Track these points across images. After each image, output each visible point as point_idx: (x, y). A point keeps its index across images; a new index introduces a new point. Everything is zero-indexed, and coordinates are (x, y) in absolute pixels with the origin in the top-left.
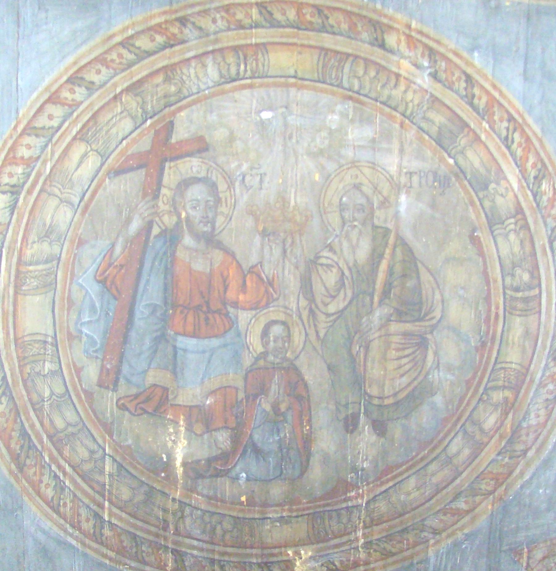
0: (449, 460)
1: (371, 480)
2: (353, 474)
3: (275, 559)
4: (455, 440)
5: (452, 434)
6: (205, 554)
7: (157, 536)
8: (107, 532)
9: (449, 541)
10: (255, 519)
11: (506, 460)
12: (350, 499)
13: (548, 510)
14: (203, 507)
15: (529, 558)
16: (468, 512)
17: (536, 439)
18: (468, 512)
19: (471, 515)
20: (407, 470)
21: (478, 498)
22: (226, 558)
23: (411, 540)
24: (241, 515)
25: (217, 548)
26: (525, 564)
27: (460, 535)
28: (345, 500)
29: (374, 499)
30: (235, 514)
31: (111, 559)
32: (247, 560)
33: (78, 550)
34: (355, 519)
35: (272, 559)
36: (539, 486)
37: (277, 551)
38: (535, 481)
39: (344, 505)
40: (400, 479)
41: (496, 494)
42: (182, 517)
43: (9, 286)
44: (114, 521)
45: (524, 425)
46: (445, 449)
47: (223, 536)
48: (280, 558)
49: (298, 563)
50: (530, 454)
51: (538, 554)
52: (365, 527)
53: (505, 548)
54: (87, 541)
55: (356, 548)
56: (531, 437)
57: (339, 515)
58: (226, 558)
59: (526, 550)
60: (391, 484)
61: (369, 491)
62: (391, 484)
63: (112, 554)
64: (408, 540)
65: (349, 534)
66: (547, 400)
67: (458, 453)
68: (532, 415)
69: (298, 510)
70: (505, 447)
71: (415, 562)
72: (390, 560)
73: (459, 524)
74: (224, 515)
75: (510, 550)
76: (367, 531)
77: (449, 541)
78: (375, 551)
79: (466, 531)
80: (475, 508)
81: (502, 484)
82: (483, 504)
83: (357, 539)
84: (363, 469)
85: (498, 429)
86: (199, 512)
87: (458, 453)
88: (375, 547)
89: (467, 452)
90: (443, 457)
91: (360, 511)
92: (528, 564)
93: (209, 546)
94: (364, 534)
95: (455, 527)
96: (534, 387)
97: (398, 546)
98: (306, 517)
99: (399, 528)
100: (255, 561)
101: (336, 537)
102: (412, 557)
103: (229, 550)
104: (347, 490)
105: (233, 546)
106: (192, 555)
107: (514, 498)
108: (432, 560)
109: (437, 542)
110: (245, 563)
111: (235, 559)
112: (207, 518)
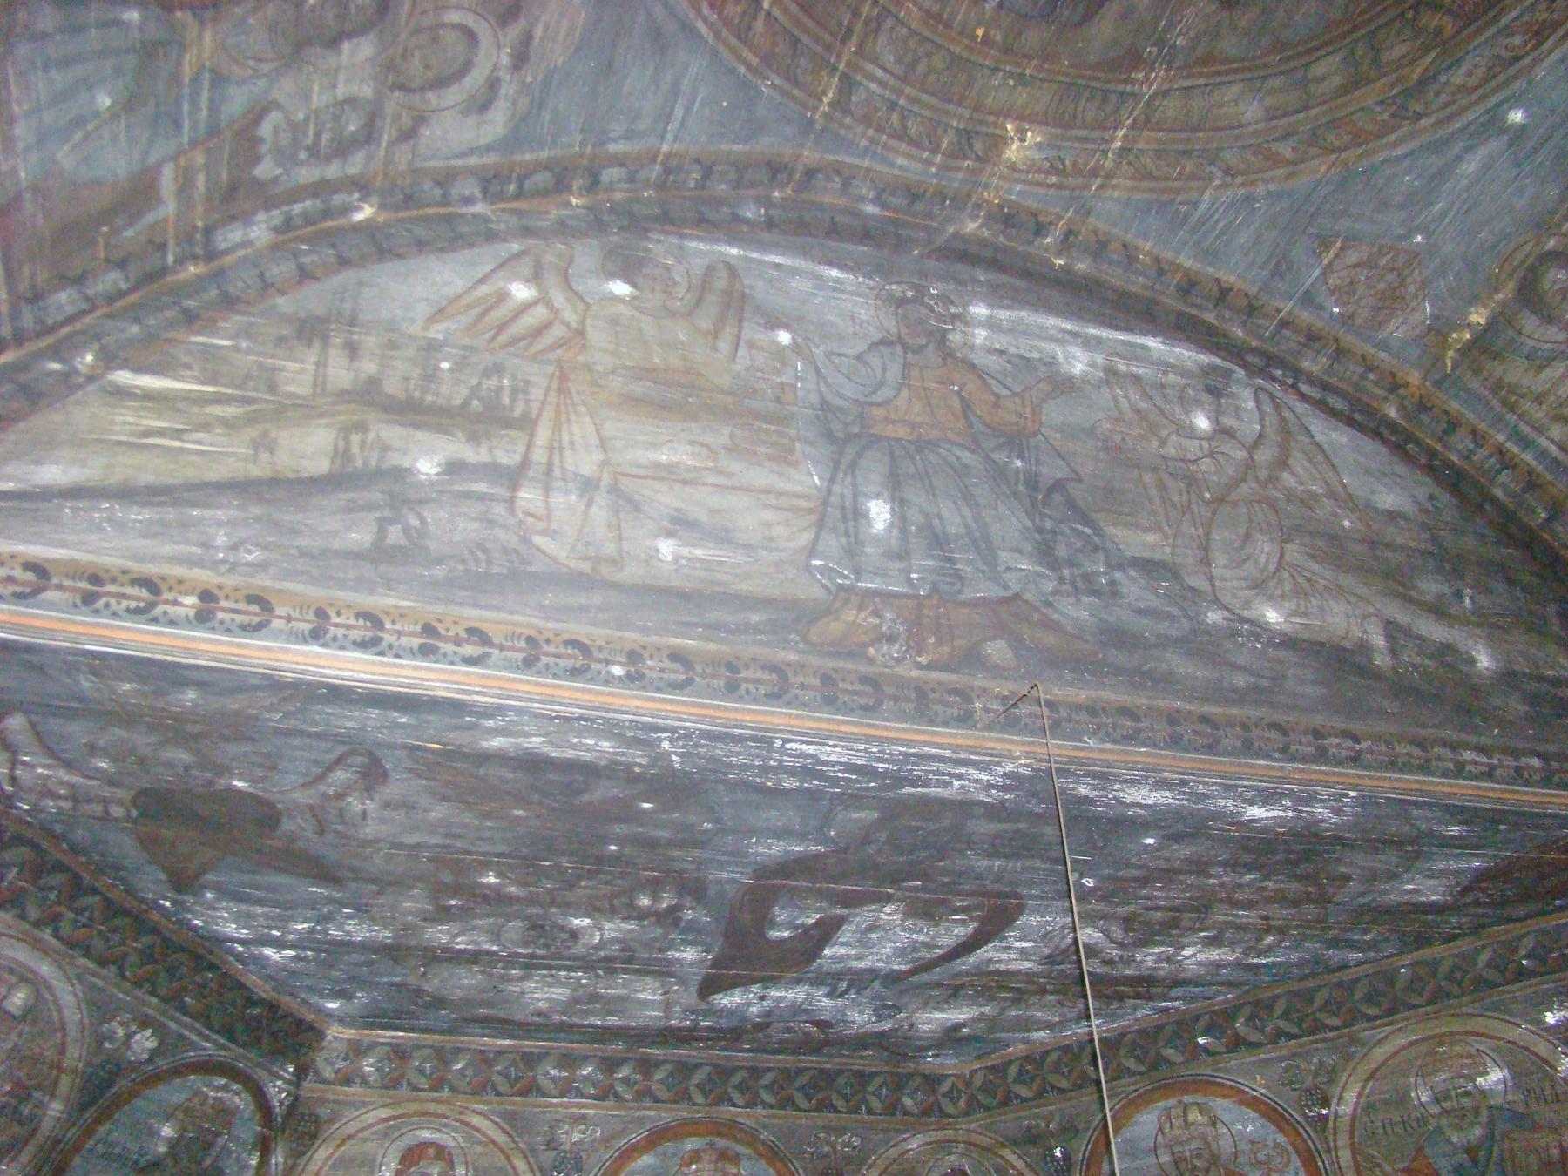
0: (1305, 83)
1: (1176, 65)
2: (1155, 49)
3: (984, 129)
4: (1329, 58)
5: (1330, 49)
6: (887, 94)
7: (828, 48)
8: (759, 26)
9: (1241, 191)
10: (982, 66)
11: (1386, 116)
12: (1133, 82)
13: (1402, 207)
14: (914, 25)
15: (1337, 256)
16: (1289, 163)
17: (1447, 105)
18: (1289, 163)
19: (1291, 169)
20: (1236, 71)
21: (1313, 151)
22: (916, 109)
23: (1188, 169)
24: (965, 55)
25: (908, 90)
26: (1325, 262)
27: (1261, 189)
28: (1126, 81)
29: (1166, 94)
30: (958, 50)
31: (749, 67)
32: (944, 120)
33: (706, 43)
34: (1124, 113)
35: (979, 129)
36: (1408, 172)
37: (991, 119)
38: (1407, 163)
39: (1121, 87)
40: (1218, 79)
41: (1343, 155)
42: (878, 30)
43: (26, 1143)
44: (776, 12)
45: (1443, 78)
46: (1307, 65)
47: (926, 76)
48: (991, 130)
49: (1014, 147)
50: (1424, 122)
51: (1352, 257)
52: (1132, 127)
53: (1311, 230)
54: (725, 33)
55: (1105, 152)
56: (1443, 98)
57: (1105, 100)
58: (916, 109)
59: (1338, 244)
60: (1202, 81)
61: (1164, 80)
62: (1202, 81)
63: (754, 60)
64: (1184, 168)
65: (1105, 129)
66: (1498, 57)
67: (1321, 80)
68: (1463, 70)
69: (1049, 71)
70: (1395, 97)
71: (1179, 199)
72: (1145, 184)
73: (1269, 174)
74: (938, 46)
75: (1318, 236)
76: (1133, 133)
77: (1241, 191)
78: (1130, 163)
79: (1272, 187)
80: (1302, 161)
81: (1360, 145)
82: (1316, 162)
83: (1112, 140)
84: (1174, 46)
85: (1401, 66)
86: (905, 31)
87: (1321, 80)
88: (1131, 158)
89: (1337, 81)
90: (1299, 75)
91: (1137, 104)
92: (1330, 264)
93: (898, 84)
94: (1125, 136)
95: (1260, 176)
96: (1493, 29)
97: (1166, 169)
98: (1055, 86)
99: (1181, 147)
100: (955, 124)
101: (1085, 128)
102: (1178, 192)
103: (924, 97)
104: (1136, 69)
105: (932, 94)
106: (868, 90)
107: (1363, 173)
108: (1203, 207)
109: (1224, 186)
110: (939, 123)
111: (928, 113)
112: (912, 43)
